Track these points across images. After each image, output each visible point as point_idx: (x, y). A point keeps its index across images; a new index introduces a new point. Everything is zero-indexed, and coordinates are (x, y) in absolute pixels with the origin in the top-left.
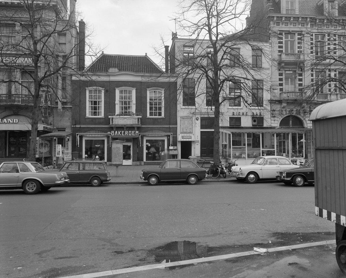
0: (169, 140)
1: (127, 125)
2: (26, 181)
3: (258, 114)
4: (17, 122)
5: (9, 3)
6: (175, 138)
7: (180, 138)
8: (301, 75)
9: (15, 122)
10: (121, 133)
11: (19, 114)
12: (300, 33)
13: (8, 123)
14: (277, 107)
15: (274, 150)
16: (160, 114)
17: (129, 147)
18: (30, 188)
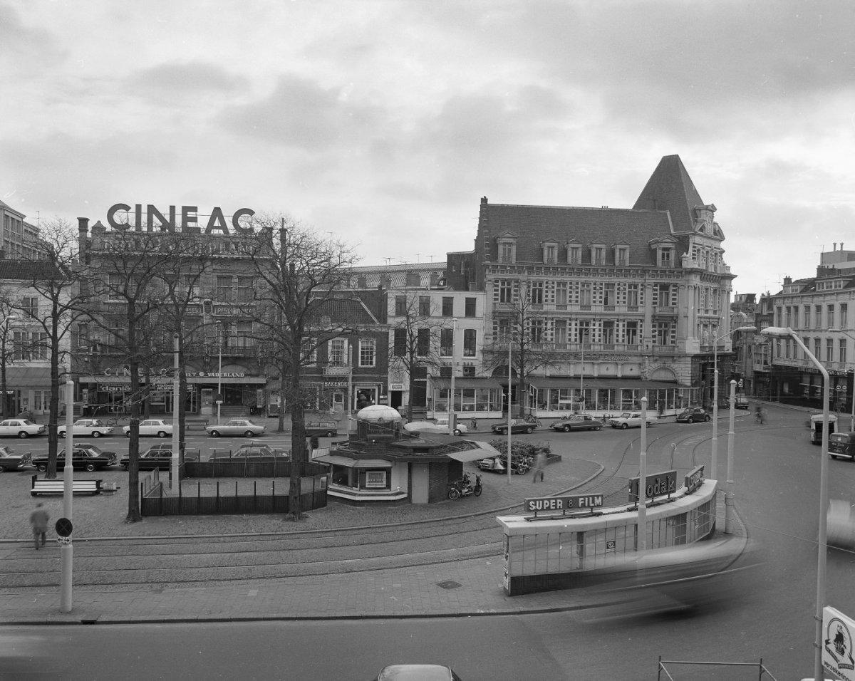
0: (379, 389)
2: (21, 432)
3: (470, 364)
6: (386, 387)
7: (390, 388)
8: (674, 327)
12: (517, 281)
14: (490, 357)
16: (371, 363)
18: (162, 434)
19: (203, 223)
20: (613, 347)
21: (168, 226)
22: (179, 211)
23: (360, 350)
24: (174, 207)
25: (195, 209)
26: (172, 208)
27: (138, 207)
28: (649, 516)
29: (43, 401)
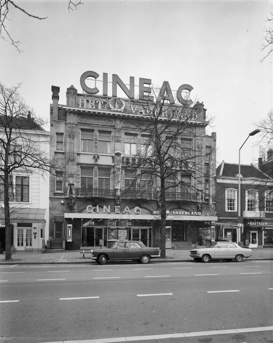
1: (257, 218)
4: (181, 214)
5: (116, 115)
9: (199, 214)
10: (256, 224)
11: (182, 208)
13: (179, 215)
15: (142, 230)
17: (255, 234)
19: (155, 95)
21: (145, 101)
22: (137, 82)
23: (247, 203)
24: (107, 74)
25: (149, 82)
26: (132, 79)
27: (105, 75)
28: (60, 300)
29: (25, 238)
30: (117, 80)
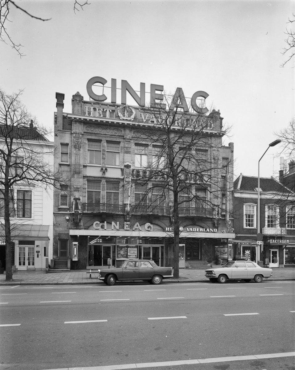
1: (278, 235)
4: (196, 230)
5: (125, 124)
9: (215, 231)
10: (277, 241)
11: (196, 224)
13: (194, 232)
15: (153, 248)
17: (276, 252)
19: (168, 102)
20: (212, 215)
22: (148, 89)
24: (115, 80)
25: (161, 88)
26: (143, 85)
27: (114, 81)
29: (27, 256)
30: (126, 86)
